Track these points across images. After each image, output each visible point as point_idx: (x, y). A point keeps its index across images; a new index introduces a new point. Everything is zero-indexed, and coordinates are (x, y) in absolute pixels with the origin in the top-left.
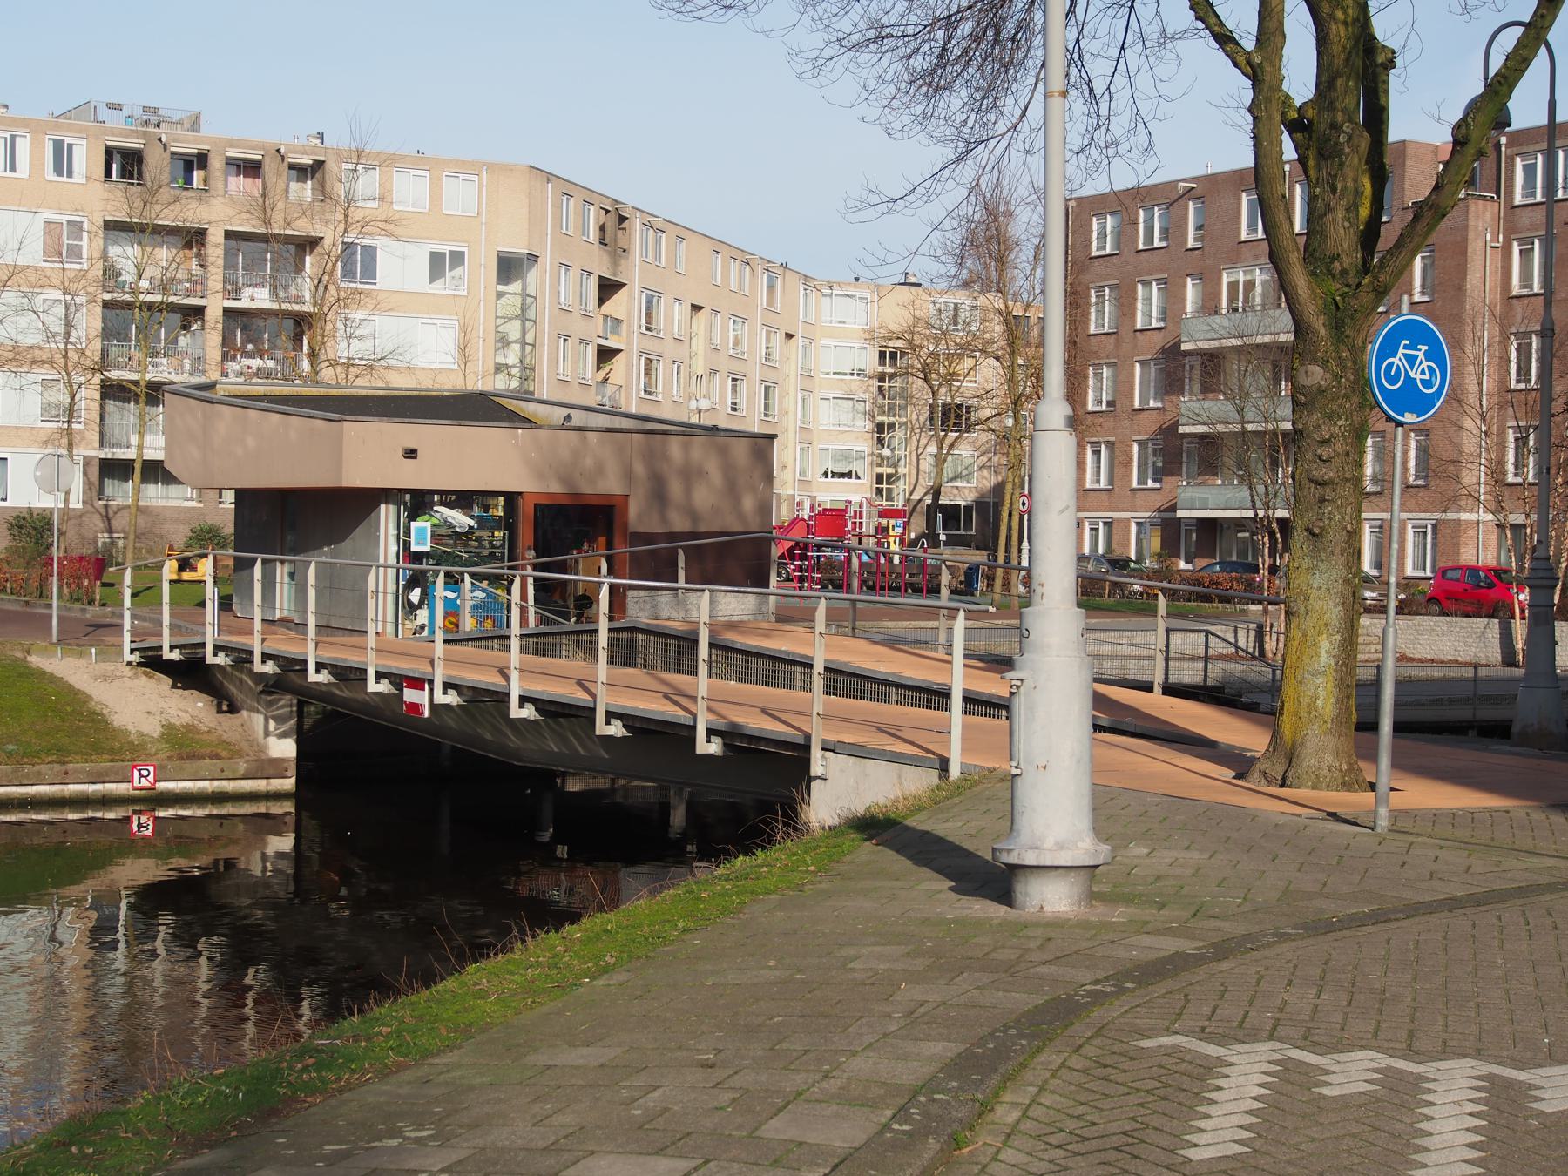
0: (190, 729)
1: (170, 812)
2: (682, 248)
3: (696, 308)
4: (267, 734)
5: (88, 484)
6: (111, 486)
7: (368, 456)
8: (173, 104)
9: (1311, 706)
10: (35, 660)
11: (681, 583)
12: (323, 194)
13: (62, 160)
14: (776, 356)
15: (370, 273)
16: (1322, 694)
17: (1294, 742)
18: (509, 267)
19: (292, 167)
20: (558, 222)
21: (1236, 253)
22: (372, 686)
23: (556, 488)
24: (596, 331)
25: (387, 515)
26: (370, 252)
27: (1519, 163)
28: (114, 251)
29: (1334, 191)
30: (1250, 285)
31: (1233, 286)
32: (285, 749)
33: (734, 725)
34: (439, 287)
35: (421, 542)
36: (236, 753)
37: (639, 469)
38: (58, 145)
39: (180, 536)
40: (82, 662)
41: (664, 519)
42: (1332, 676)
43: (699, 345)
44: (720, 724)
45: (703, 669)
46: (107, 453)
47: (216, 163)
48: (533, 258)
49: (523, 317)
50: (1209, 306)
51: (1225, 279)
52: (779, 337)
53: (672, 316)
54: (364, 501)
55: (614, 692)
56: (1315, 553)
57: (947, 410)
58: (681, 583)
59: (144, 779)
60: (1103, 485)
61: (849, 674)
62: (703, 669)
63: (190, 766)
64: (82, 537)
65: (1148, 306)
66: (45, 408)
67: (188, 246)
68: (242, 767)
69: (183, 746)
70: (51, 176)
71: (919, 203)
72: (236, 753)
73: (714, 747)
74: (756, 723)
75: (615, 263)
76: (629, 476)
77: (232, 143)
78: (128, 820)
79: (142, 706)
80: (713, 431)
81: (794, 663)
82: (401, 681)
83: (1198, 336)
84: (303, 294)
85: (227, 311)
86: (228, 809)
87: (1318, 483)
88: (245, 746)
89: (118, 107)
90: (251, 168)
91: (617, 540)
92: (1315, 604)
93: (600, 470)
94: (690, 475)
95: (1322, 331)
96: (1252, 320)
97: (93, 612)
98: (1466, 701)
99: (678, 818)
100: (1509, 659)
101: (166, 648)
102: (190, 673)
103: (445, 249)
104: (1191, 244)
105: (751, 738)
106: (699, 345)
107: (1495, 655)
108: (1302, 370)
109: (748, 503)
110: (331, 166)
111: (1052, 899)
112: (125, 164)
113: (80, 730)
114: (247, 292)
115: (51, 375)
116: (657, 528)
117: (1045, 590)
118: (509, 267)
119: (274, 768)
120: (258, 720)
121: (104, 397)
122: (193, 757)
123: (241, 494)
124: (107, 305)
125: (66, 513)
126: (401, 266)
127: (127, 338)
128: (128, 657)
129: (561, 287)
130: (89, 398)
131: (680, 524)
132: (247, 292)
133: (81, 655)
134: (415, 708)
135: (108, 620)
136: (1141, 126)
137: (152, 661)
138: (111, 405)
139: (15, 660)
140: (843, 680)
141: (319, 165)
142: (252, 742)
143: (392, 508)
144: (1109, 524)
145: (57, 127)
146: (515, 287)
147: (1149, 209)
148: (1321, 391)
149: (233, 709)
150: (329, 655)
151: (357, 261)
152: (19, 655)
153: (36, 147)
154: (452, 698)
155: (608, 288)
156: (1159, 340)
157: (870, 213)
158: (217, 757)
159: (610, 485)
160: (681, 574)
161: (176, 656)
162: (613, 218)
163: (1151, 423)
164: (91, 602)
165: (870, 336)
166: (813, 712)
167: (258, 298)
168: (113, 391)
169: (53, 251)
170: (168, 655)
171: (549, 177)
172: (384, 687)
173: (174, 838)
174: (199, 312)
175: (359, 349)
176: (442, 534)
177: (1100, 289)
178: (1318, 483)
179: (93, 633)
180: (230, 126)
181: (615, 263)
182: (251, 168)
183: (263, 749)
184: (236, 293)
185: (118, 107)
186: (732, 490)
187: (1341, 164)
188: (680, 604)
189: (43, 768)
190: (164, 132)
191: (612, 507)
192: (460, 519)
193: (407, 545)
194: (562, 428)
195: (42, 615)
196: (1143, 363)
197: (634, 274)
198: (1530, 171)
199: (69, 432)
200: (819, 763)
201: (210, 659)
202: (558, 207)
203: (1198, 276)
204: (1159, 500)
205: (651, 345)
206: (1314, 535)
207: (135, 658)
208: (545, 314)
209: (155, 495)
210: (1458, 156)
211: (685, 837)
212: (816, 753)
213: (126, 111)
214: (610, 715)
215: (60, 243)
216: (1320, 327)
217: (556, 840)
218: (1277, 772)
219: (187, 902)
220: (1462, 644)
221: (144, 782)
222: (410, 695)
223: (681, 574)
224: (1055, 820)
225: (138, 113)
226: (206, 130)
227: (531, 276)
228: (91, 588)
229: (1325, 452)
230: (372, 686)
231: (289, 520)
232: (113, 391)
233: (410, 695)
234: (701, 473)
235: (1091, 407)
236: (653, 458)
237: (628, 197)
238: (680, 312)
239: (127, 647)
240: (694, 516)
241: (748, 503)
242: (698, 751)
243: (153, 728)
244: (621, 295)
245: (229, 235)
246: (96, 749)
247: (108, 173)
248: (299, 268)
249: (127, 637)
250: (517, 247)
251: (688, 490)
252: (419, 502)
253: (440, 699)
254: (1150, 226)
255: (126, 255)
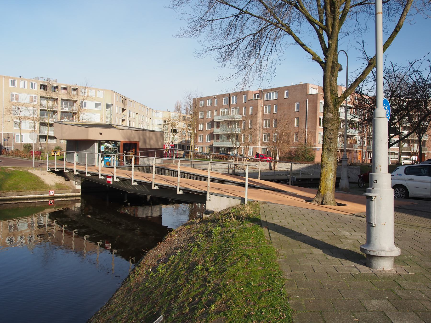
0: (60, 184)
1: (57, 200)
2: (134, 104)
3: (137, 114)
4: (76, 185)
5: (37, 139)
6: (41, 140)
7: (93, 134)
8: (52, 78)
9: (328, 187)
10: (30, 171)
11: (155, 157)
12: (77, 94)
13: (33, 86)
14: (148, 121)
15: (85, 106)
16: (330, 184)
17: (324, 195)
18: (108, 106)
19: (72, 89)
20: (116, 99)
21: (222, 107)
22: (100, 177)
23: (127, 140)
24: (122, 117)
25: (96, 144)
26: (85, 103)
27: (265, 94)
28: (42, 101)
29: (333, 76)
30: (224, 111)
31: (222, 112)
32: (79, 187)
33: (187, 188)
34: (96, 109)
35: (103, 149)
36: (69, 188)
37: (141, 137)
38: (32, 84)
39: (53, 148)
40: (39, 171)
41: (146, 146)
42: (332, 180)
43: (137, 119)
44: (183, 188)
45: (179, 176)
46: (41, 134)
47: (59, 88)
48: (112, 105)
49: (110, 114)
50: (218, 115)
51: (220, 111)
52: (149, 119)
53: (133, 115)
54: (92, 142)
55: (135, 176)
56: (329, 154)
57: (174, 130)
58: (155, 157)
59: (52, 194)
60: (201, 141)
61: (197, 175)
62: (179, 176)
63: (60, 191)
64: (36, 148)
65: (209, 115)
66: (30, 127)
67: (55, 101)
68: (71, 191)
69: (59, 187)
70: (31, 88)
71: (234, 79)
72: (69, 188)
73: (181, 192)
74: (191, 188)
75: (125, 106)
76: (139, 138)
77: (62, 84)
78: (49, 201)
79: (51, 180)
80: (154, 131)
81: (185, 173)
82: (106, 176)
83: (216, 119)
84: (75, 108)
85: (61, 112)
86: (68, 199)
87: (330, 139)
88: (71, 187)
89: (43, 78)
90: (65, 89)
91: (137, 150)
92: (329, 165)
93: (135, 137)
94: (150, 138)
95: (332, 106)
96: (225, 117)
97: (40, 161)
98: (272, 175)
99: (149, 197)
100: (271, 169)
101: (56, 169)
102: (60, 173)
103: (98, 103)
104: (215, 105)
105: (190, 191)
106: (137, 119)
107: (268, 168)
108: (327, 114)
109: (160, 143)
110: (79, 89)
111: (386, 266)
112: (44, 87)
113: (39, 184)
114: (65, 109)
115: (31, 121)
116: (144, 147)
117: (381, 168)
118: (108, 106)
119: (77, 191)
120: (74, 182)
121: (40, 125)
122: (61, 189)
123: (68, 141)
124: (41, 110)
125: (35, 144)
126: (90, 105)
127: (44, 115)
128: (48, 170)
129: (116, 109)
130: (38, 125)
131: (148, 147)
132: (65, 109)
133: (38, 170)
134: (109, 182)
135: (43, 163)
136: (273, 66)
137: (53, 171)
138: (41, 126)
139: (26, 171)
140: (183, 174)
141: (77, 89)
142: (73, 186)
143: (97, 143)
144: (202, 147)
145: (32, 80)
146: (109, 109)
147: (208, 100)
148: (331, 119)
149: (69, 180)
150: (91, 171)
151: (83, 104)
152: (26, 170)
153: (28, 84)
154: (118, 180)
155: (123, 110)
156: (210, 120)
157: (221, 81)
158: (66, 189)
159: (136, 140)
160: (155, 156)
161: (58, 170)
162: (124, 100)
163: (208, 133)
164: (39, 159)
165: (162, 119)
166: (207, 187)
167: (66, 109)
168: (41, 124)
169: (31, 100)
170: (56, 170)
171: (115, 92)
172: (102, 177)
173: (58, 204)
174: (57, 112)
175: (84, 117)
176: (107, 148)
177: (208, 111)
178: (330, 139)
179: (40, 165)
180: (61, 82)
181: (125, 106)
182: (65, 89)
183: (75, 187)
184: (63, 109)
185: (43, 78)
186: (157, 141)
187: (335, 71)
188: (148, 160)
189: (32, 192)
190: (51, 82)
191: (136, 144)
192: (109, 145)
193: (100, 150)
194: (128, 130)
195: (30, 162)
196: (208, 123)
197: (127, 108)
198: (267, 96)
199: (34, 131)
200: (209, 197)
201: (65, 171)
202: (116, 97)
203: (216, 110)
204: (210, 144)
205: (130, 119)
206: (329, 150)
207: (49, 170)
208: (114, 113)
209: (49, 141)
210: (369, 67)
211: (150, 201)
212: (208, 195)
213: (44, 79)
214: (155, 185)
215: (32, 99)
216: (332, 105)
217: (128, 202)
218: (320, 201)
219: (60, 216)
220: (262, 166)
221: (52, 194)
222: (108, 179)
223: (155, 156)
224: (385, 242)
225: (46, 79)
226: (57, 82)
227: (112, 107)
228: (39, 156)
229: (332, 132)
230: (100, 177)
231: (76, 145)
232: (41, 124)
233: (108, 179)
234: (152, 138)
235: (199, 129)
236: (143, 135)
237: (127, 97)
238: (134, 114)
239: (48, 168)
240: (151, 146)
241: (160, 143)
242: (178, 193)
243: (53, 184)
244: (125, 111)
245: (62, 99)
246: (42, 188)
247: (41, 89)
248: (74, 105)
249: (48, 166)
250: (109, 103)
251: (150, 141)
252: (101, 142)
253: (115, 180)
254: (209, 102)
255: (44, 102)
